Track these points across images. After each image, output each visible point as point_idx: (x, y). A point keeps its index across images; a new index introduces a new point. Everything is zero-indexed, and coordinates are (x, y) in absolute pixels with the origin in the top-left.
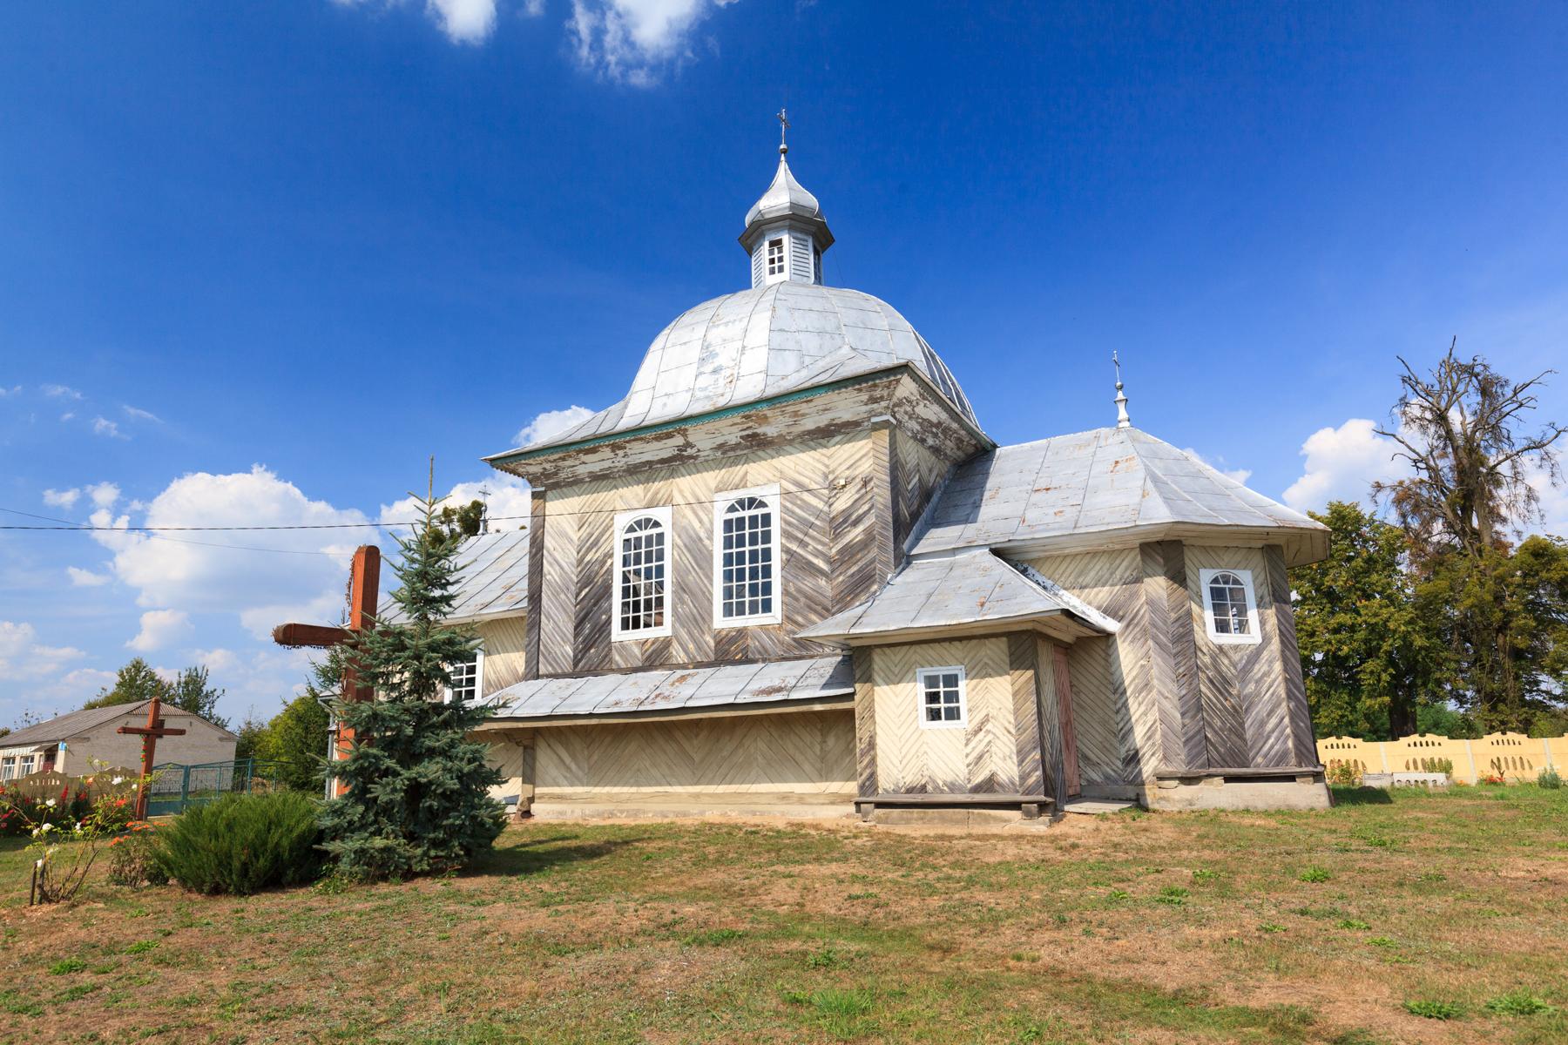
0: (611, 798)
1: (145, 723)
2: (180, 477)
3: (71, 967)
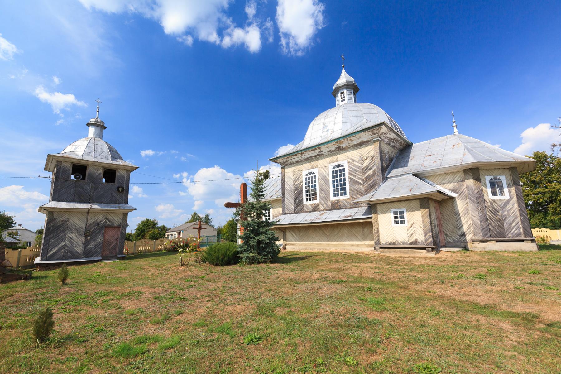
0: (306, 245)
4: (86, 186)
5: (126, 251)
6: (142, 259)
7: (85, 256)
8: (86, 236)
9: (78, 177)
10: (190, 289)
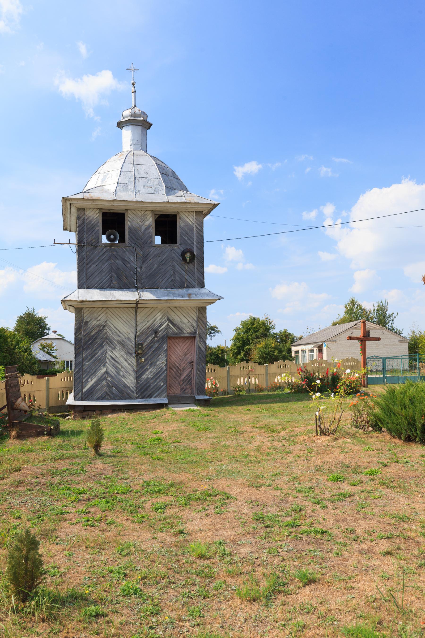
1: (359, 333)
2: (364, 193)
3: (338, 478)
4: (127, 253)
5: (214, 387)
6: (240, 408)
7: (141, 395)
8: (138, 356)
9: (112, 237)
10: (340, 505)
